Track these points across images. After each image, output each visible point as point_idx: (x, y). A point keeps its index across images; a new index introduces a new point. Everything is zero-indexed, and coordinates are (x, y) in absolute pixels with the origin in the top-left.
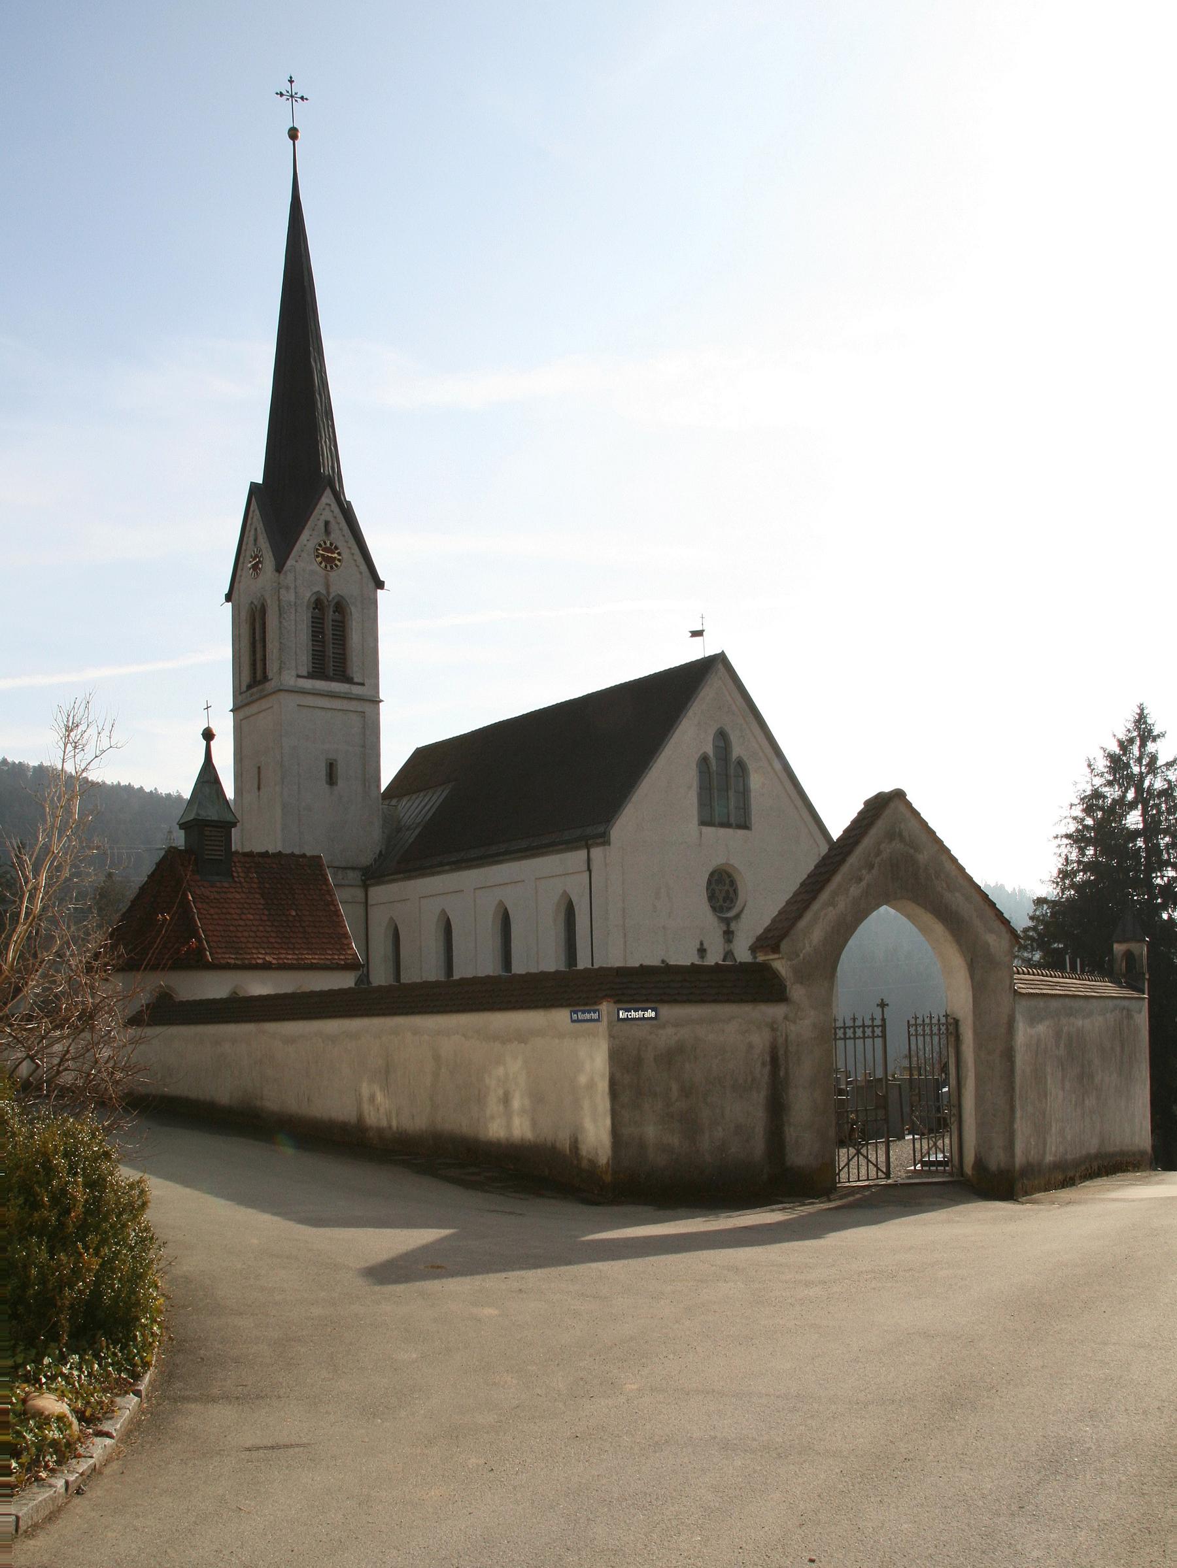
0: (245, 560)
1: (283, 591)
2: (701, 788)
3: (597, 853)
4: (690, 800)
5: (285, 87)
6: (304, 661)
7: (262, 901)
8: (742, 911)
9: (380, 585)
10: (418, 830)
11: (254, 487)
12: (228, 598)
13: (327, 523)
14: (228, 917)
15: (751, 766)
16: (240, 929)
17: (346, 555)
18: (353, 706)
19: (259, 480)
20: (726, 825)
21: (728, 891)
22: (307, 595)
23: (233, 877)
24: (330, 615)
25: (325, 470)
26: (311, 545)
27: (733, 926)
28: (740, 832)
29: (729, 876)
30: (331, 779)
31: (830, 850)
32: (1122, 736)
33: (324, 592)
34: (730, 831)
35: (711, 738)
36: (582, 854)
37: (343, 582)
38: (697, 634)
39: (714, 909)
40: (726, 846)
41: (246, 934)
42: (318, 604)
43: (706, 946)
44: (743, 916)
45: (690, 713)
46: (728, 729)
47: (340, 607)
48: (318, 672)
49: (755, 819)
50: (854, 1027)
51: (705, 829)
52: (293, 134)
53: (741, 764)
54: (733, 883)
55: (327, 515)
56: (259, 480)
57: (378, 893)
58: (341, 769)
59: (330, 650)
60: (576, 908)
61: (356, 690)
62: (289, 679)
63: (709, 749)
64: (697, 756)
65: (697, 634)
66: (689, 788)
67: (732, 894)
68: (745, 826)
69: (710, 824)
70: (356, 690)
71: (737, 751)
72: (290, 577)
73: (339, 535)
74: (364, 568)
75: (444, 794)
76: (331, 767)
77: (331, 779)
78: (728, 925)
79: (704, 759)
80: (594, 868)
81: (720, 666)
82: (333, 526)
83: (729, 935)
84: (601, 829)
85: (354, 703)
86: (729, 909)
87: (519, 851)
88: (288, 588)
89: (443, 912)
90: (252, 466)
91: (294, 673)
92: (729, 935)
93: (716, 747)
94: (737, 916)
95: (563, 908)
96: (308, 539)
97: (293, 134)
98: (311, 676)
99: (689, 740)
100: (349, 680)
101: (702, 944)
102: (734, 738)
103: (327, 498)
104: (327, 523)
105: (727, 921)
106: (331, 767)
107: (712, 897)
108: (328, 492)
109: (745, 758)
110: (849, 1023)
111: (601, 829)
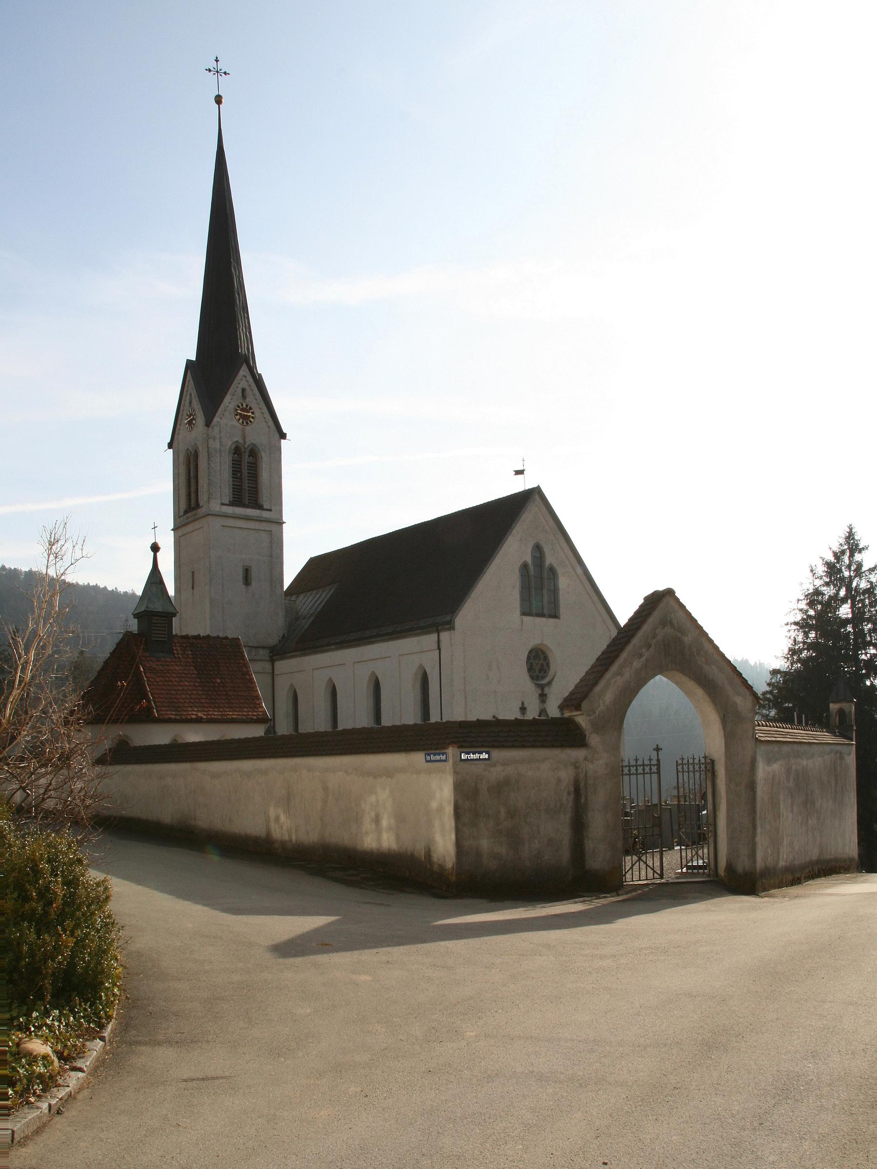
0: (183, 417)
1: (211, 441)
2: (523, 587)
3: (445, 636)
4: (514, 597)
5: (212, 65)
6: (226, 493)
7: (195, 672)
8: (553, 679)
9: (283, 436)
10: (312, 619)
11: (189, 363)
12: (170, 446)
13: (243, 390)
14: (170, 683)
15: (560, 571)
16: (179, 692)
17: (258, 414)
18: (263, 526)
19: (193, 358)
20: (541, 615)
21: (542, 665)
22: (229, 444)
23: (174, 654)
24: (246, 459)
25: (243, 350)
26: (232, 406)
27: (546, 690)
28: (552, 620)
29: (543, 653)
30: (247, 581)
31: (618, 633)
32: (836, 549)
33: (241, 441)
34: (544, 620)
35: (529, 550)
36: (434, 637)
37: (256, 434)
38: (519, 472)
39: (532, 677)
40: (541, 631)
41: (183, 696)
42: (237, 451)
43: (526, 705)
44: (554, 683)
45: (514, 532)
46: (543, 544)
47: (254, 453)
48: (237, 501)
49: (562, 611)
50: (636, 766)
51: (525, 618)
52: (218, 100)
53: (552, 570)
54: (546, 658)
55: (244, 384)
56: (193, 358)
57: (282, 666)
58: (254, 573)
59: (246, 485)
60: (429, 677)
61: (265, 514)
62: (215, 507)
63: (528, 559)
64: (519, 564)
65: (519, 472)
66: (514, 587)
67: (545, 667)
68: (555, 616)
69: (529, 614)
70: (265, 514)
71: (549, 560)
72: (216, 430)
73: (253, 399)
74: (271, 423)
75: (331, 592)
76: (247, 572)
77: (247, 581)
78: (543, 690)
79: (525, 566)
80: (443, 647)
81: (537, 497)
82: (248, 392)
83: (543, 697)
84: (448, 618)
85: (264, 524)
86: (543, 678)
87: (387, 634)
88: (214, 438)
89: (330, 680)
90: (188, 348)
91: (219, 502)
92: (543, 697)
93: (533, 557)
94: (549, 683)
95: (419, 677)
96: (230, 402)
97: (218, 100)
98: (232, 504)
99: (513, 552)
100: (260, 507)
101: (523, 704)
102: (547, 550)
103: (244, 371)
104: (243, 390)
105: (542, 687)
106: (247, 572)
107: (530, 669)
108: (244, 367)
109: (555, 565)
110: (633, 763)
111: (448, 618)
